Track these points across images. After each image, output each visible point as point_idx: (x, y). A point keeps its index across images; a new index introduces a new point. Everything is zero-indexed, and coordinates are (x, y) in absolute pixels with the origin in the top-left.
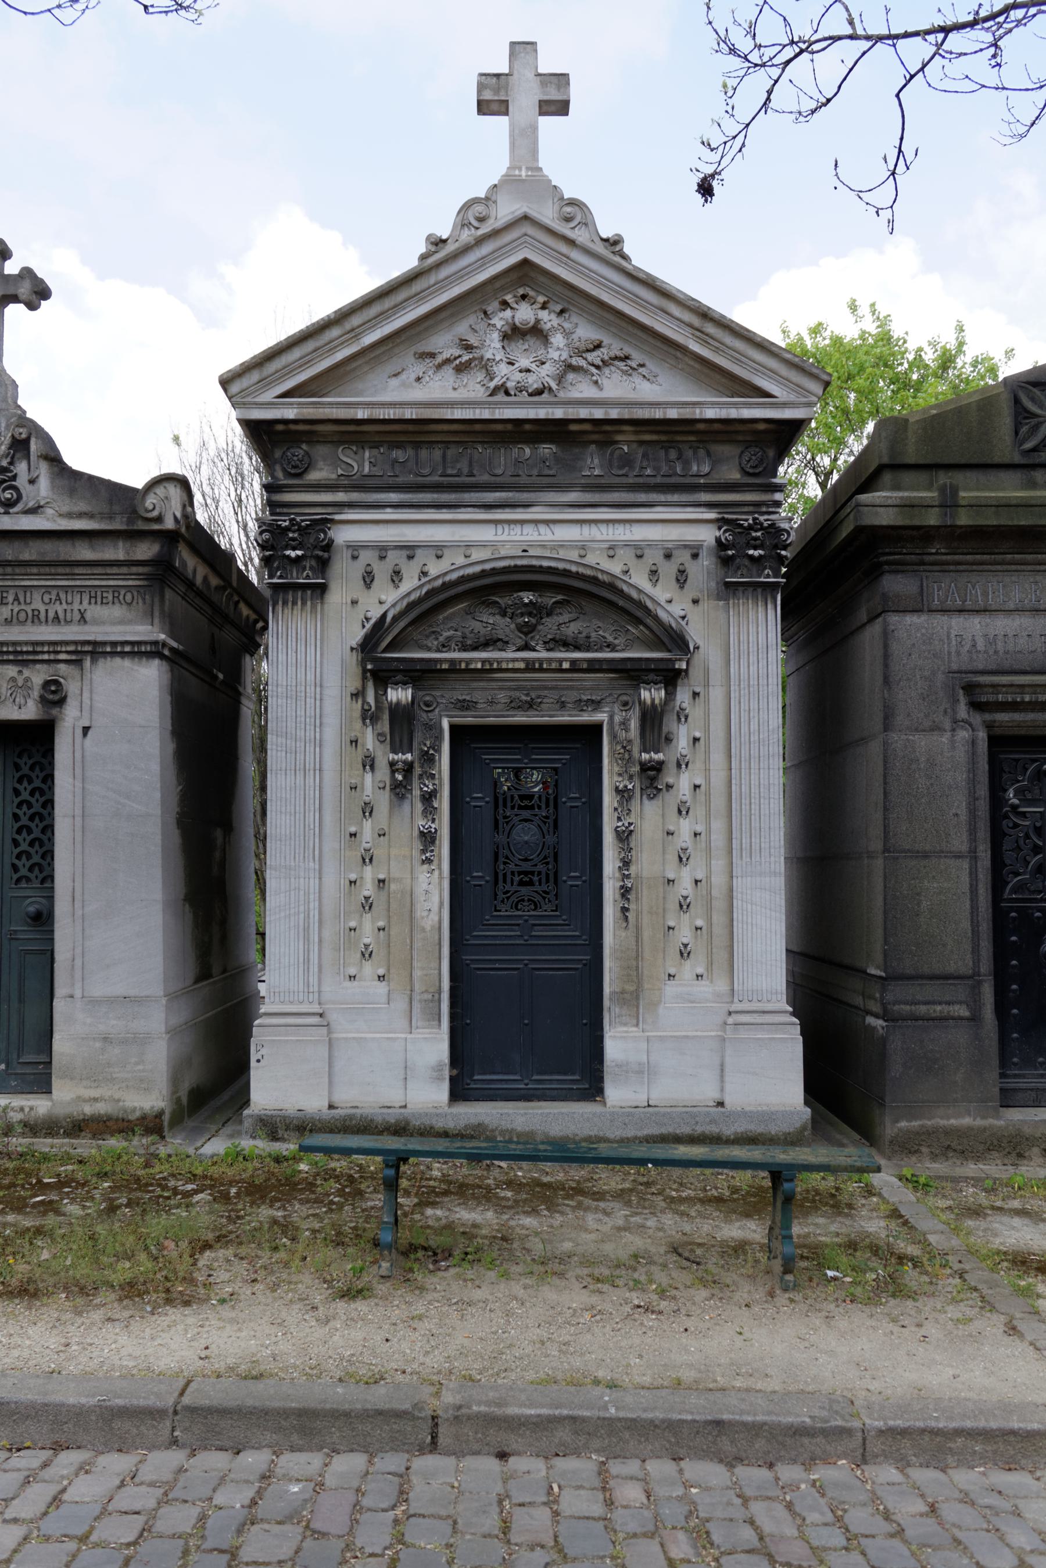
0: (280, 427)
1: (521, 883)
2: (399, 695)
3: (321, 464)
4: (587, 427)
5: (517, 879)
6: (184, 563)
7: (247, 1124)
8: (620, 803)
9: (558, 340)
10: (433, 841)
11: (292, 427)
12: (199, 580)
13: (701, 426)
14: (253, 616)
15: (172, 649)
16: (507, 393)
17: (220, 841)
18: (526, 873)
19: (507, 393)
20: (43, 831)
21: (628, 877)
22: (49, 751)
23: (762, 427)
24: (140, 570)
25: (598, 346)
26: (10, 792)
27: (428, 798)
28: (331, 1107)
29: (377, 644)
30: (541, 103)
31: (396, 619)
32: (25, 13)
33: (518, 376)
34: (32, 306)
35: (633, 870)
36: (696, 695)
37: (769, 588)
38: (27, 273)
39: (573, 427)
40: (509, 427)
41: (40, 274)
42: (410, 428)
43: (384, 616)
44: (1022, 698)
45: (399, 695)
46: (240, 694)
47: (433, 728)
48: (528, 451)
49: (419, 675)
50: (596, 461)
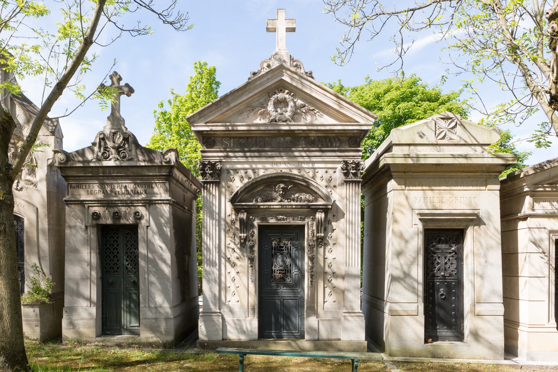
0: (205, 132)
1: (280, 273)
2: (244, 216)
3: (218, 144)
4: (301, 132)
5: (278, 272)
6: (176, 175)
7: (198, 345)
8: (310, 249)
9: (291, 104)
10: (253, 261)
11: (209, 132)
12: (180, 180)
13: (337, 132)
14: (196, 188)
15: (173, 202)
16: (276, 121)
17: (187, 259)
18: (281, 270)
19: (276, 121)
20: (135, 257)
21: (313, 271)
22: (136, 233)
23: (355, 132)
24: (163, 177)
25: (304, 106)
26: (125, 252)
27: (252, 247)
28: (223, 339)
29: (236, 200)
30: (287, 28)
31: (241, 192)
32: (115, 23)
33: (279, 116)
34: (128, 95)
35: (314, 269)
36: (334, 216)
37: (359, 182)
38: (127, 85)
39: (296, 132)
40: (276, 132)
41: (131, 86)
42: (246, 132)
43: (238, 192)
44: (284, 139)
45: (244, 216)
46: (192, 213)
47: (253, 226)
48: (282, 139)
49: (250, 211)
50: (304, 142)
